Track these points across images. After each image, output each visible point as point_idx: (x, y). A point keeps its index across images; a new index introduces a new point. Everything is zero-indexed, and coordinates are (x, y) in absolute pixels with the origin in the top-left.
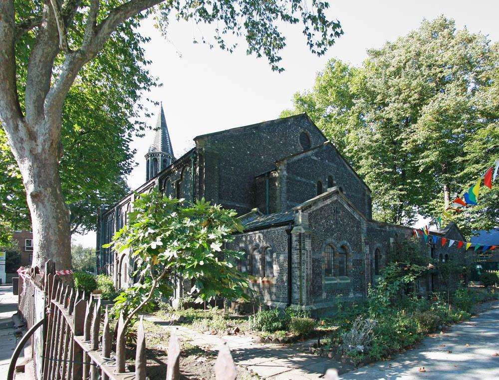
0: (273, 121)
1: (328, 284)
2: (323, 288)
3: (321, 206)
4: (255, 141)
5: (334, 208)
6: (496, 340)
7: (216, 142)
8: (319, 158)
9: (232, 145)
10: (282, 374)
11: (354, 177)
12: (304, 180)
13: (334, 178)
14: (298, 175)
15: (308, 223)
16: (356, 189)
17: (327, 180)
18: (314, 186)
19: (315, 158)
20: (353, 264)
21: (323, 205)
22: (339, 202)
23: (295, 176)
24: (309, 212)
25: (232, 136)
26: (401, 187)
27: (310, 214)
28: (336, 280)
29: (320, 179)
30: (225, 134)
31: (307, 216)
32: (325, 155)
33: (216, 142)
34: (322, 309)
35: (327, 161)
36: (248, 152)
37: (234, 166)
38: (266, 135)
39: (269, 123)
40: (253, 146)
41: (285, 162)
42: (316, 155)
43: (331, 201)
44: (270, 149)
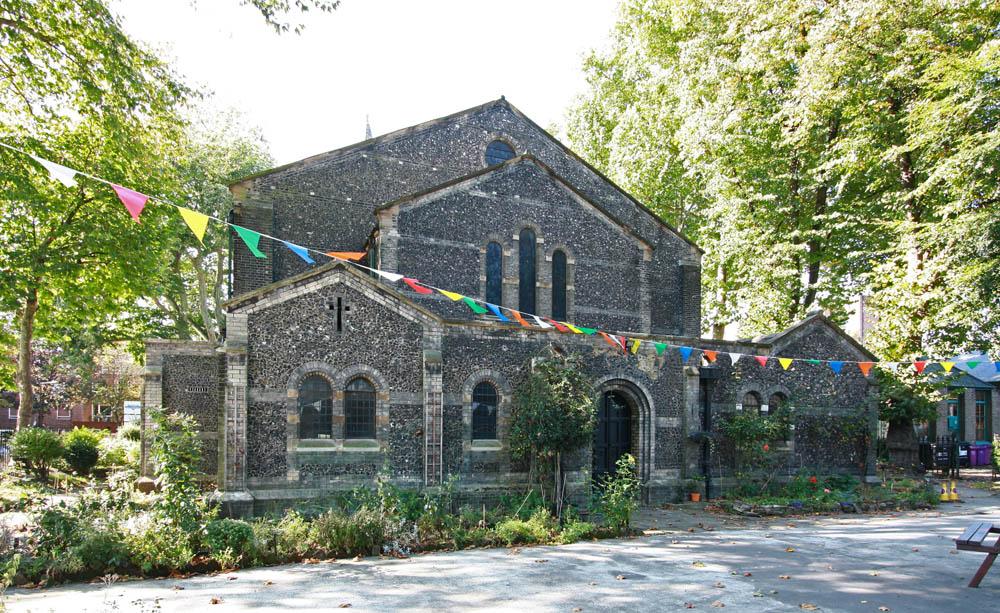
0: (414, 128)
1: (302, 454)
2: (289, 461)
3: (287, 298)
4: (366, 175)
5: (331, 299)
6: (622, 605)
7: (273, 188)
8: (495, 193)
9: (311, 188)
10: (296, 611)
11: (605, 225)
12: (445, 243)
13: (538, 231)
14: (428, 234)
15: (246, 334)
16: (608, 251)
17: (516, 237)
18: (476, 254)
19: (483, 194)
20: (391, 414)
21: (295, 295)
22: (348, 287)
23: (422, 236)
24: (251, 311)
25: (309, 173)
26: (796, 233)
27: (252, 317)
28: (331, 445)
29: (494, 236)
30: (294, 169)
31: (246, 321)
32: (511, 184)
33: (273, 188)
34: (277, 500)
35: (517, 197)
36: (349, 199)
37: (314, 229)
38: (394, 159)
39: (403, 133)
40: (361, 186)
41: (396, 210)
42: (485, 187)
43: (319, 287)
44: (405, 187)
